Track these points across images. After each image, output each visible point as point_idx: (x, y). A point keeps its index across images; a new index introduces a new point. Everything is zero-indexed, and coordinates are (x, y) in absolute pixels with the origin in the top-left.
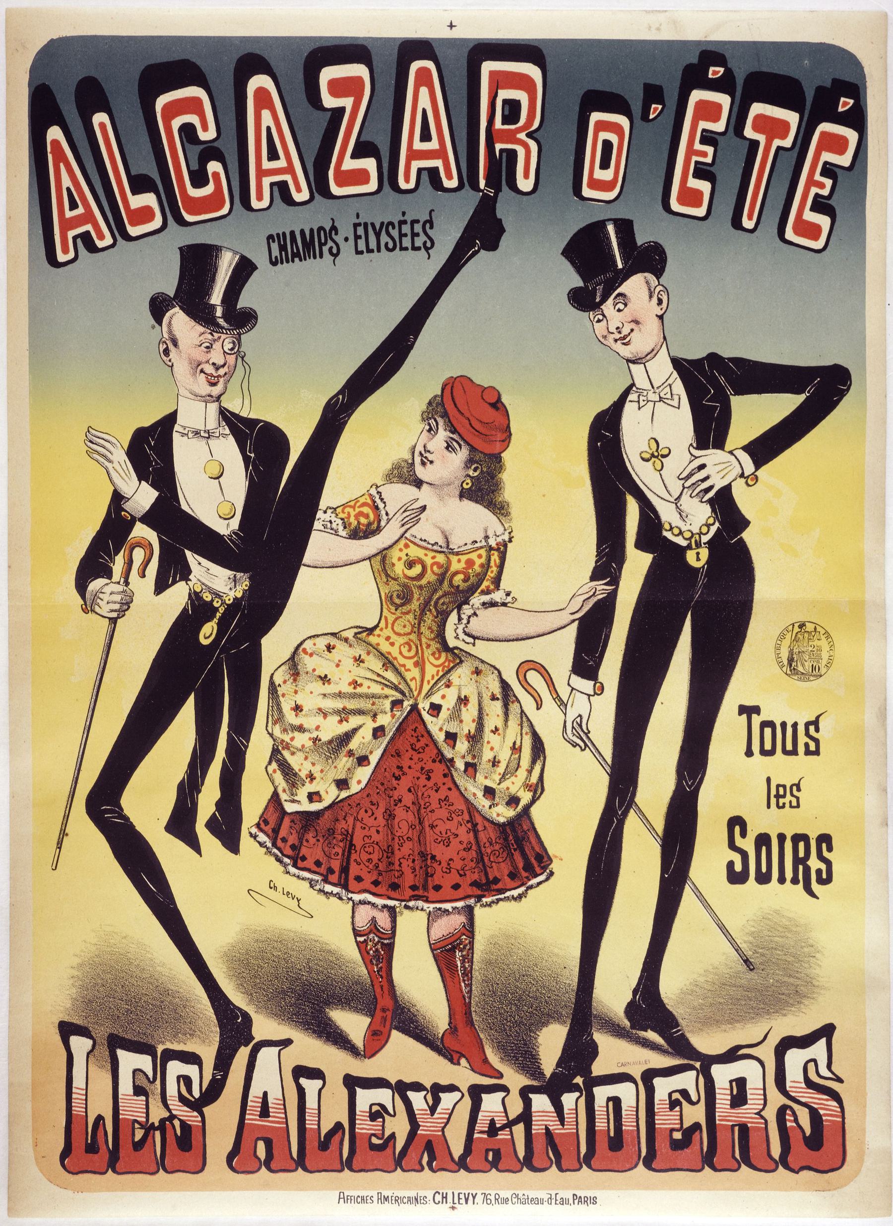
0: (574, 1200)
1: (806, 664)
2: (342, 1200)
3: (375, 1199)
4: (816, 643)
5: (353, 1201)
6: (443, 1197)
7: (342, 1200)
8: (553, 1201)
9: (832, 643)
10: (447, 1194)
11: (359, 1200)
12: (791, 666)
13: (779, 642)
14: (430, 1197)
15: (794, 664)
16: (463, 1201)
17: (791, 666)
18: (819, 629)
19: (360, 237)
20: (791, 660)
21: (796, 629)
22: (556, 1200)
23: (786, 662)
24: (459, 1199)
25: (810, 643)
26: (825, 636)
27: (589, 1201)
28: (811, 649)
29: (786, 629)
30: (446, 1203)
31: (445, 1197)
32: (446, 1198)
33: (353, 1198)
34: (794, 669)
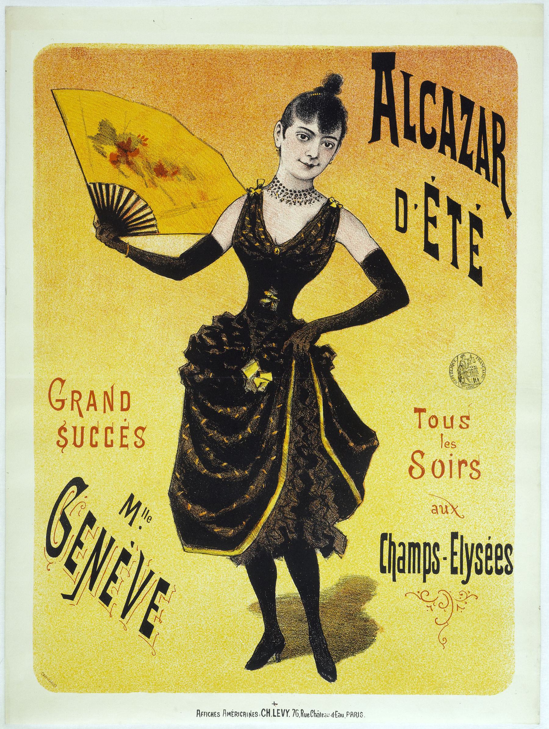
0: (347, 714)
1: (470, 378)
2: (198, 715)
3: (221, 714)
4: (473, 364)
5: (206, 715)
6: (267, 712)
7: (198, 715)
8: (335, 716)
9: (482, 363)
10: (269, 710)
11: (242, 714)
12: (460, 381)
13: (451, 369)
14: (259, 713)
15: (462, 380)
16: (280, 715)
17: (460, 381)
18: (473, 356)
19: (456, 554)
20: (460, 379)
21: (460, 359)
22: (336, 715)
23: (458, 380)
24: (278, 713)
25: (470, 366)
26: (477, 359)
27: (357, 715)
28: (470, 369)
29: (454, 360)
30: (269, 716)
31: (268, 712)
32: (269, 713)
33: (206, 713)
34: (463, 383)
